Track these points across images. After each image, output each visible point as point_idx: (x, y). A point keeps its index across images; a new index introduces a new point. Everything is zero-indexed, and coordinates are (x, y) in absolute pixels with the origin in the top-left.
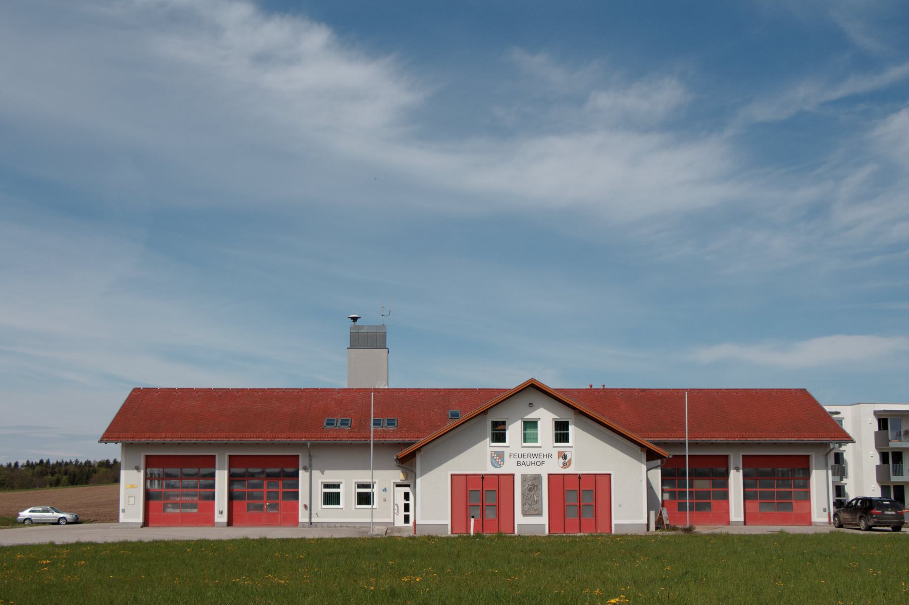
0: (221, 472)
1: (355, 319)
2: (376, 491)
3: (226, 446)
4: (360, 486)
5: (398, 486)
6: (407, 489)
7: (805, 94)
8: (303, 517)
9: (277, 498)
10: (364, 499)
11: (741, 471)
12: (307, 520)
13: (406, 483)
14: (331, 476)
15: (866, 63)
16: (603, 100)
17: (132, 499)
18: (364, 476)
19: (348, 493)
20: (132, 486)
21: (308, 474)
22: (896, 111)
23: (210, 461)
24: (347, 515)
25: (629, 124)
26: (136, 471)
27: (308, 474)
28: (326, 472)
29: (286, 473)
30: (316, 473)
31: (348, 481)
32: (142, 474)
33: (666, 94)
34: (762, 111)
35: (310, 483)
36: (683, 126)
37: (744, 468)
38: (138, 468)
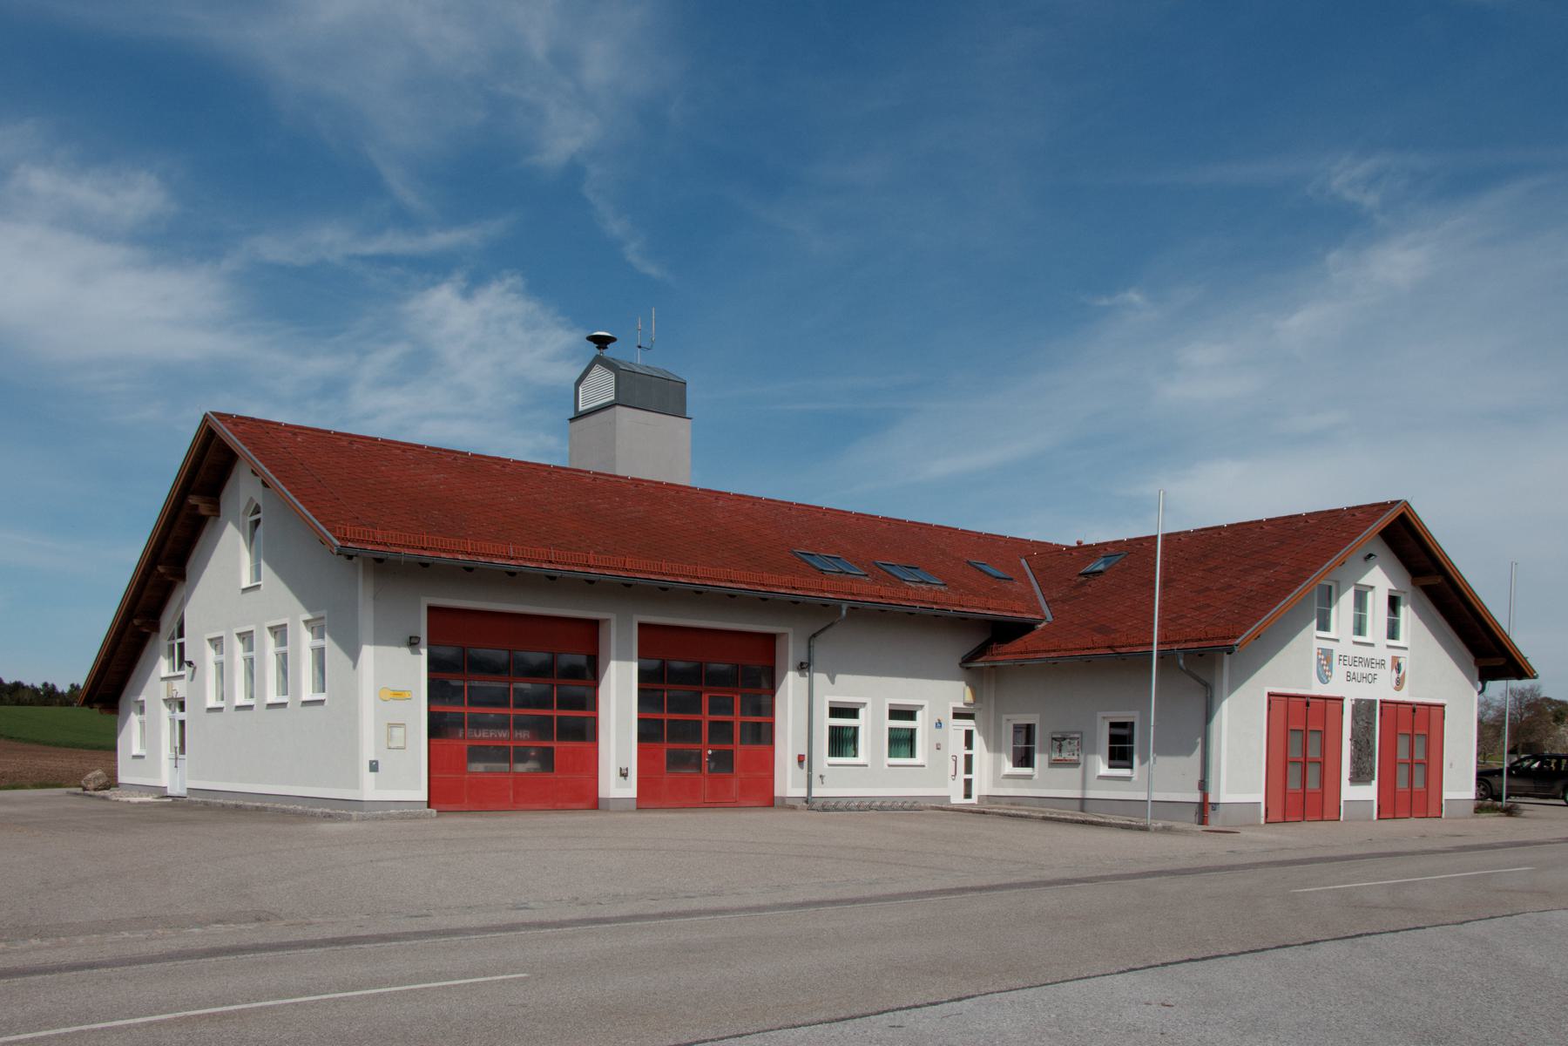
0: (624, 664)
1: (602, 342)
2: (921, 724)
3: (626, 591)
4: (895, 714)
5: (957, 716)
6: (969, 724)
7: (332, 240)
8: (788, 782)
9: (730, 737)
10: (902, 742)
11: (424, 652)
12: (803, 793)
13: (970, 710)
14: (848, 688)
15: (404, 219)
16: (41, 180)
17: (398, 732)
18: (903, 690)
19: (872, 728)
20: (398, 695)
21: (805, 680)
22: (434, 284)
23: (588, 636)
24: (870, 773)
25: (78, 223)
26: (406, 651)
27: (805, 680)
28: (839, 678)
29: (758, 680)
30: (820, 678)
31: (875, 696)
32: (634, 666)
33: (139, 195)
34: (273, 249)
35: (799, 704)
36: (163, 243)
37: (430, 644)
38: (413, 643)
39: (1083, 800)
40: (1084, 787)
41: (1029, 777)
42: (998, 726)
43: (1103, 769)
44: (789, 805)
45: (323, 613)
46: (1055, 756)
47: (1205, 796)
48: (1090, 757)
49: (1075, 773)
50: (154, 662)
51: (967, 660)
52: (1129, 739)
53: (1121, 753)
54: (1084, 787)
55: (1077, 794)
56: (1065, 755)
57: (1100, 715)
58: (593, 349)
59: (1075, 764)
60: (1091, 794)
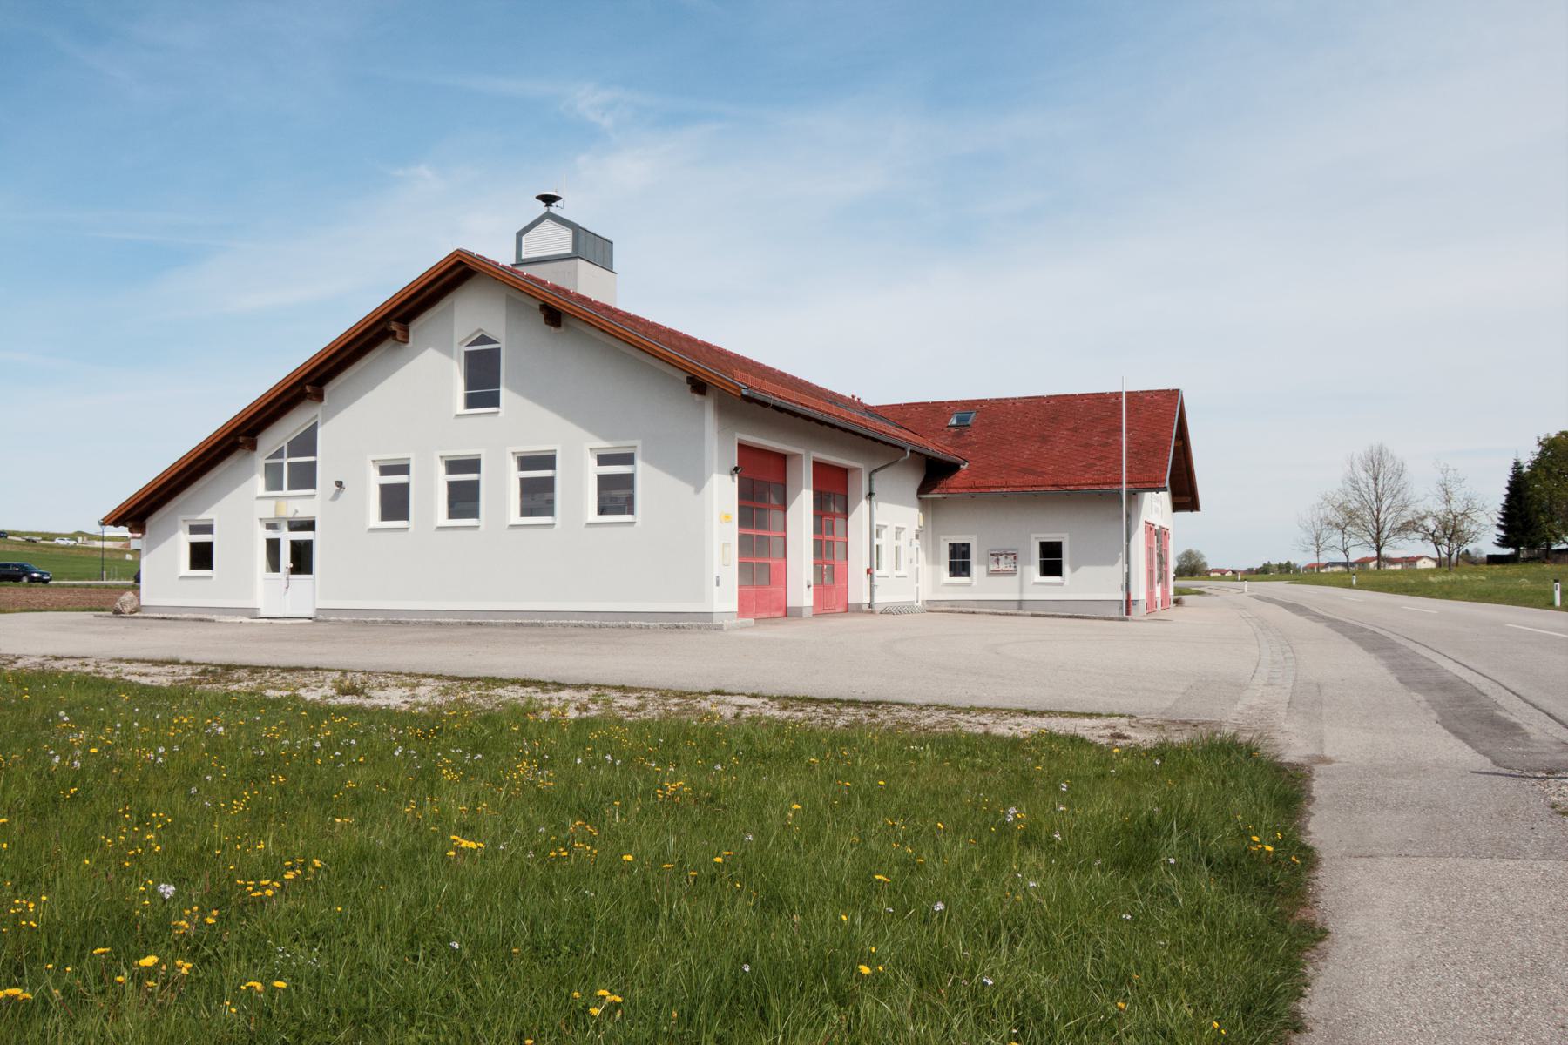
1: (549, 200)
39: (1020, 601)
40: (1021, 591)
41: (969, 585)
42: (936, 545)
43: (1037, 577)
44: (859, 609)
45: (9, 668)
46: (993, 567)
47: (1128, 595)
48: (1026, 568)
49: (1014, 580)
50: (174, 531)
51: (923, 489)
52: (966, 554)
53: (1051, 561)
54: (1021, 591)
55: (1016, 597)
56: (1002, 567)
57: (1033, 536)
58: (541, 207)
59: (1013, 573)
60: (1027, 597)
